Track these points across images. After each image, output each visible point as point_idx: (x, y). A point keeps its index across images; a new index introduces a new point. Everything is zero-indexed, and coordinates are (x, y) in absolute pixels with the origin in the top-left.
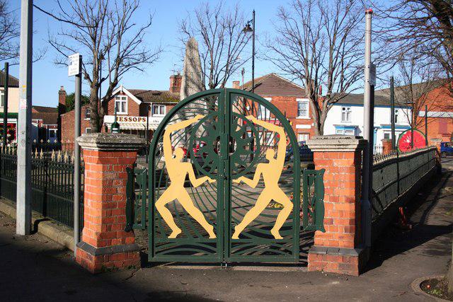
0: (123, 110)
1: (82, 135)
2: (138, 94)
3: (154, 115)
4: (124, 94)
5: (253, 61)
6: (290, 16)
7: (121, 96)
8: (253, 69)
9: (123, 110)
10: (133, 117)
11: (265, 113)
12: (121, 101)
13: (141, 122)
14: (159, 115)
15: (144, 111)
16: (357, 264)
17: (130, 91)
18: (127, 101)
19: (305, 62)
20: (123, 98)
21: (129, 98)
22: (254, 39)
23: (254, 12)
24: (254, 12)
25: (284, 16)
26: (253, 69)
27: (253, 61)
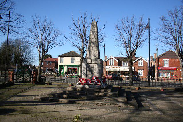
0: (112, 64)
1: (11, 81)
2: (117, 59)
3: (124, 66)
4: (113, 58)
5: (149, 40)
6: (167, 19)
7: (111, 59)
8: (149, 43)
9: (112, 64)
10: (115, 67)
11: (9, 72)
12: (111, 61)
13: (118, 68)
14: (125, 66)
15: (120, 64)
16: (155, 77)
17: (115, 58)
18: (113, 61)
19: (175, 39)
20: (112, 60)
21: (114, 60)
22: (149, 39)
23: (149, 19)
24: (149, 19)
25: (163, 19)
26: (149, 43)
27: (149, 40)
